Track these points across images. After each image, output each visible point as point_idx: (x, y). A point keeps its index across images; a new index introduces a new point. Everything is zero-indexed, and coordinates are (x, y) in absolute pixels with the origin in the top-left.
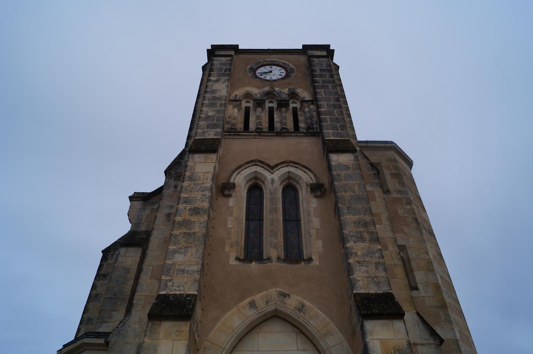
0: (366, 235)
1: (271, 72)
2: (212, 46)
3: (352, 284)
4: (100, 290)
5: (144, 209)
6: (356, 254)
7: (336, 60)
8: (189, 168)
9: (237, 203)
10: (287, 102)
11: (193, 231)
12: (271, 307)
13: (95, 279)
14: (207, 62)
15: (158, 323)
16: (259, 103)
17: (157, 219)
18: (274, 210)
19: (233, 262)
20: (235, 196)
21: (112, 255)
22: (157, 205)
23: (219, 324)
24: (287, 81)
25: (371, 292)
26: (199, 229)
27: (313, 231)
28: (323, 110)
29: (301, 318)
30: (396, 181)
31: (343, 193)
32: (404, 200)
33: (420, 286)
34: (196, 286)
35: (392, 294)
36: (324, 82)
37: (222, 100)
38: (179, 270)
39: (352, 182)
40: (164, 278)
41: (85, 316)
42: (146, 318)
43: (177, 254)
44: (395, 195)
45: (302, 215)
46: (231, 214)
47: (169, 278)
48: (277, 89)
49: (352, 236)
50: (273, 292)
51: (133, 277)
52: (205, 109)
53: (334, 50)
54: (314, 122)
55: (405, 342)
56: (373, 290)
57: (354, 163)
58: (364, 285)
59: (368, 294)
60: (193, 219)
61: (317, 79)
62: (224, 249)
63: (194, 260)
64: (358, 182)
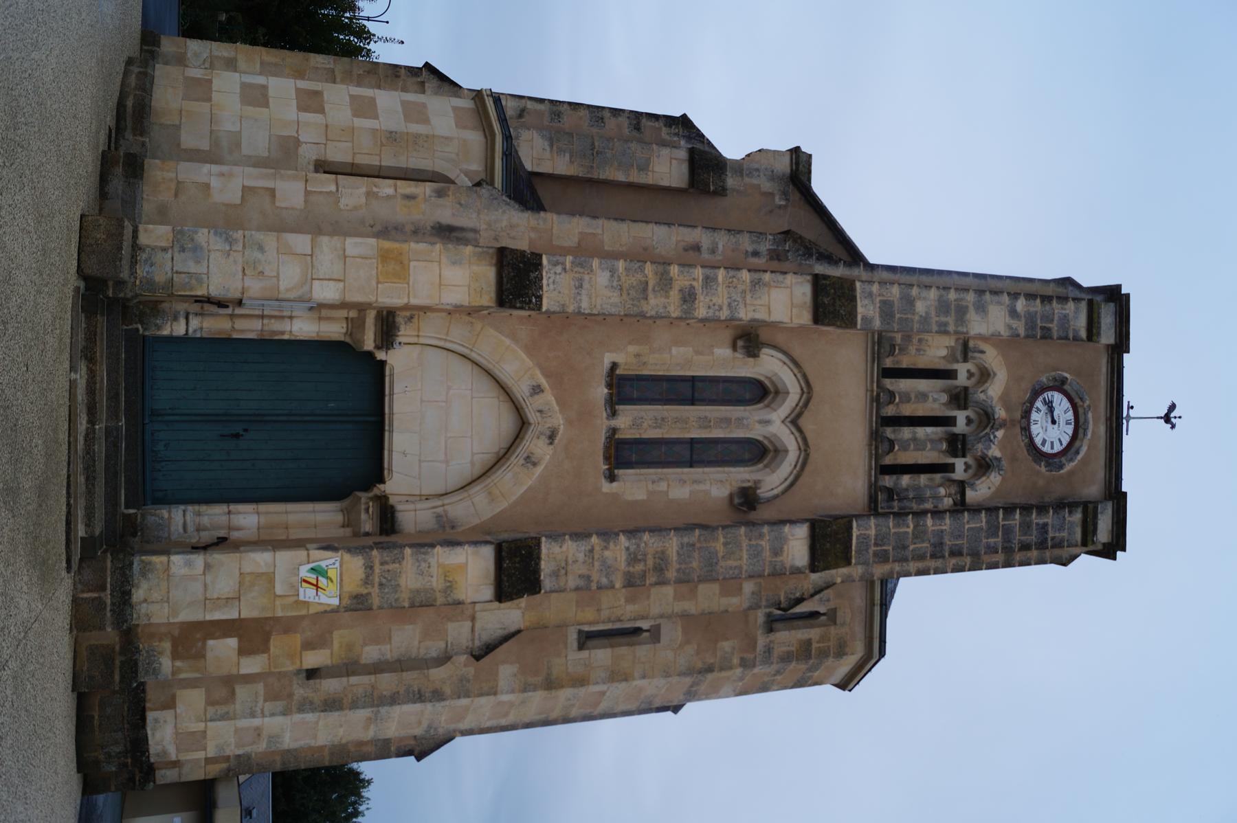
0: (639, 567)
1: (1054, 422)
2: (1128, 296)
3: (555, 537)
4: (611, 123)
5: (773, 177)
6: (606, 548)
7: (1086, 562)
8: (780, 277)
9: (721, 361)
10: (960, 453)
11: (651, 296)
12: (532, 416)
13: (632, 112)
14: (1085, 285)
15: (494, 261)
16: (960, 398)
17: (689, 230)
18: (705, 423)
19: (608, 359)
20: (734, 358)
21: (677, 134)
22: (783, 203)
23: (508, 342)
24: (1023, 453)
25: (543, 563)
26: (654, 304)
27: (663, 486)
28: (929, 522)
29: (516, 460)
30: (793, 649)
31: (722, 540)
32: (750, 656)
33: (585, 654)
34: (556, 308)
35: (539, 592)
36: (1008, 531)
37: (956, 326)
38: (581, 280)
39: (745, 556)
40: (569, 259)
41: (566, 106)
42: (499, 246)
43: (609, 274)
44: (762, 641)
45: (700, 470)
46: (697, 353)
47: (568, 267)
48: (1000, 434)
49: (638, 546)
50: (558, 420)
51: (631, 179)
52: (933, 294)
53: (1115, 559)
54: (906, 503)
55: (462, 597)
56: (546, 567)
57: (788, 566)
58: (551, 554)
59: (539, 558)
60: (674, 295)
61: (1017, 516)
62: (630, 343)
63: (599, 302)
64: (745, 568)
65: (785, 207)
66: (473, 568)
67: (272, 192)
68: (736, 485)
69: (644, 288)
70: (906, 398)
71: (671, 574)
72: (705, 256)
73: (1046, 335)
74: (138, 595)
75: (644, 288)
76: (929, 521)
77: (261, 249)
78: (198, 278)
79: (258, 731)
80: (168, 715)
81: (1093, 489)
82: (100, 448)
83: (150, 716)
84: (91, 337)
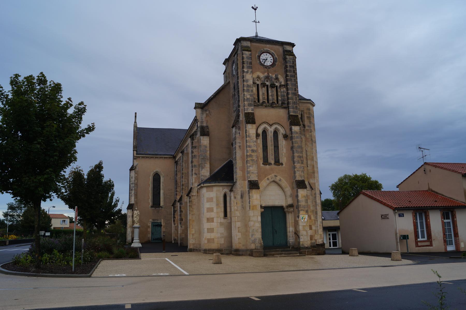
3: (295, 177)
12: (273, 180)
19: (262, 165)
26: (254, 158)
27: (283, 154)
48: (270, 75)
50: (273, 175)
58: (298, 178)
60: (253, 154)
65: (209, 111)
66: (302, 193)
67: (238, 228)
68: (283, 139)
69: (252, 160)
70: (264, 98)
71: (301, 155)
72: (241, 145)
73: (251, 63)
74: (306, 246)
75: (252, 160)
76: (289, 96)
77: (254, 229)
78: (259, 239)
79: (320, 225)
80: (317, 241)
81: (280, 49)
82: (286, 253)
83: (317, 243)
84: (271, 255)
